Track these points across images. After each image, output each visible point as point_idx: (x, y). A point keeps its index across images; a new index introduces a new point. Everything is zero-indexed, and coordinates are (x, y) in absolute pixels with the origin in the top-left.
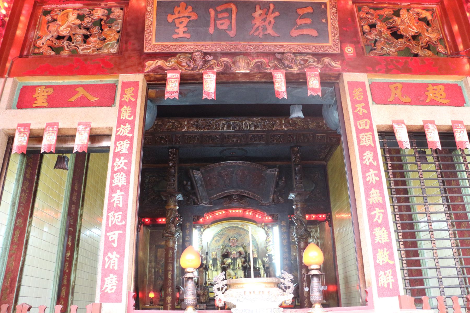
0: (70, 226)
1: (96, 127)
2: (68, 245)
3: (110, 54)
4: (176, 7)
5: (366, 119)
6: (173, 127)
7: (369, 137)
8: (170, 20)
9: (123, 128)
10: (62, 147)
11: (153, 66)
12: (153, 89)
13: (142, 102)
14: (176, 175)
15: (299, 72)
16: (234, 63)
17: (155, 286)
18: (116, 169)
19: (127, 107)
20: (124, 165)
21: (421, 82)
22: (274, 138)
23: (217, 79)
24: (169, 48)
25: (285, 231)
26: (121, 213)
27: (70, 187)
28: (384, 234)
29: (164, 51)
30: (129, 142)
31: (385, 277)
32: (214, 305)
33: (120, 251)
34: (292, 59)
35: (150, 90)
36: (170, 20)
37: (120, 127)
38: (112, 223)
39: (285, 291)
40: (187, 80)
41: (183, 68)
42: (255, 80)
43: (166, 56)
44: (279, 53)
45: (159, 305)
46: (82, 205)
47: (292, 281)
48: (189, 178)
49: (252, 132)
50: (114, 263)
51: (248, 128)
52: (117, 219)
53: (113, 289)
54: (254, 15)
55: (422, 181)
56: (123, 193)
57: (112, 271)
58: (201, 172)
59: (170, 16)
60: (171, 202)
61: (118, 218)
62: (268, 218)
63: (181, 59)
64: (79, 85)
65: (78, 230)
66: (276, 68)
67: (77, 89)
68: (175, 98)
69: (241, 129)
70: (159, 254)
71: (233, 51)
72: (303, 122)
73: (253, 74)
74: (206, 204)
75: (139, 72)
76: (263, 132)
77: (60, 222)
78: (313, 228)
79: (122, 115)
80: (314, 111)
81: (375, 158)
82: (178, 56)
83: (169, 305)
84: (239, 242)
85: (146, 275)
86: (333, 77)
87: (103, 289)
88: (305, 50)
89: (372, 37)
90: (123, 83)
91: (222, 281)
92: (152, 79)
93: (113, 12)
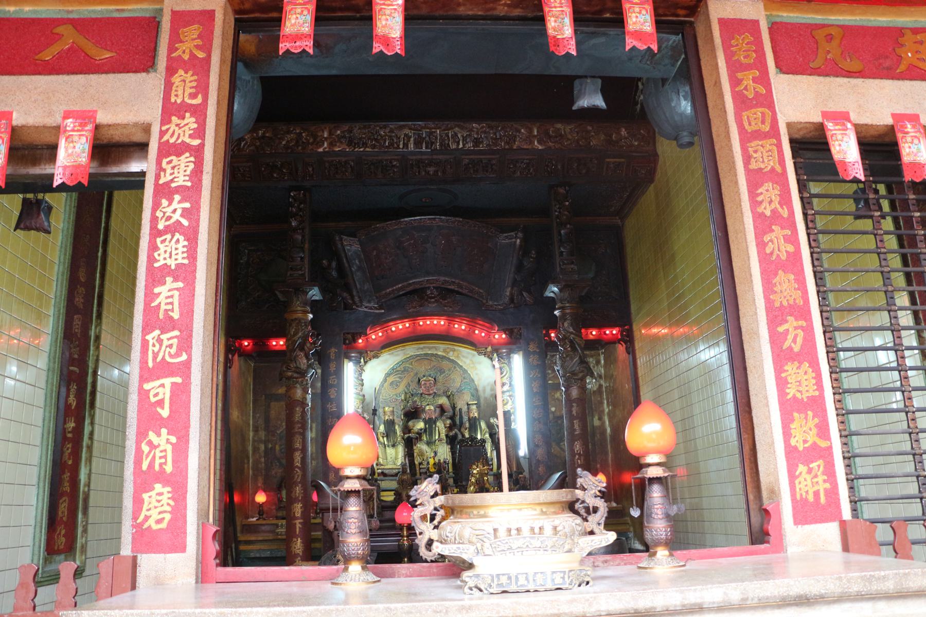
0: (72, 362)
1: (110, 123)
2: (68, 406)
5: (761, 107)
6: (297, 142)
7: (770, 151)
9: (177, 125)
10: (27, 176)
12: (250, 32)
13: (222, 61)
14: (306, 246)
17: (267, 478)
18: (161, 226)
19: (186, 73)
20: (182, 216)
21: (885, 25)
22: (515, 166)
25: (535, 363)
26: (176, 333)
27: (66, 276)
28: (806, 377)
30: (192, 159)
31: (808, 477)
32: (394, 520)
33: (178, 425)
35: (242, 37)
37: (170, 122)
38: (155, 358)
39: (586, 520)
40: (334, 10)
42: (496, 13)
45: (277, 518)
46: (99, 316)
47: (603, 495)
48: (335, 254)
49: (469, 152)
50: (165, 457)
51: (461, 146)
52: (168, 349)
53: (164, 518)
55: (882, 256)
56: (180, 285)
57: (161, 477)
58: (359, 240)
60: (297, 306)
61: (171, 346)
62: (499, 337)
64: (62, 19)
65: (90, 371)
67: (59, 30)
69: (445, 147)
70: (273, 414)
72: (578, 133)
74: (371, 309)
76: (493, 152)
77: (46, 355)
78: (592, 356)
80: (627, 95)
81: (785, 199)
83: (297, 522)
84: (439, 385)
85: (248, 458)
87: (139, 521)
91: (432, 497)
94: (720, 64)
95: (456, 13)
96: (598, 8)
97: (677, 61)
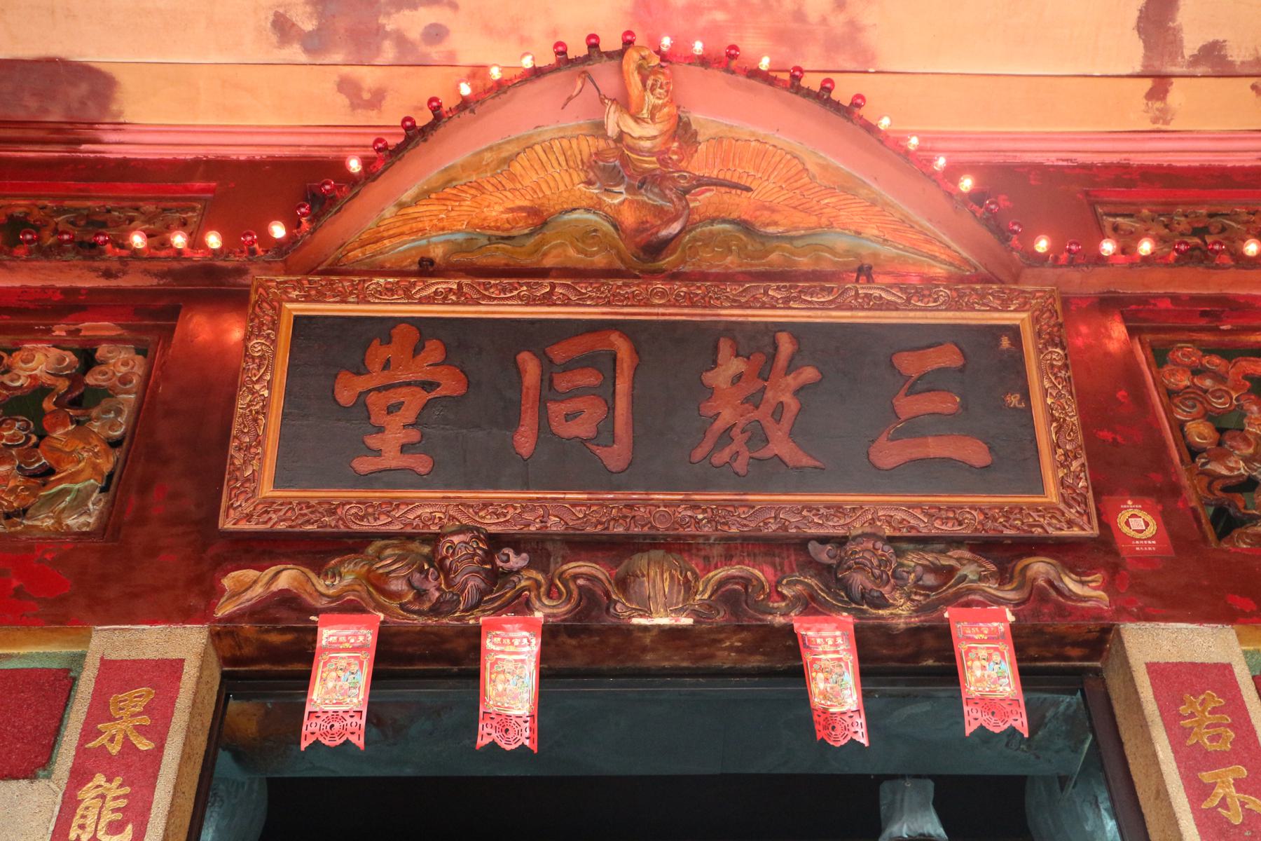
3: (62, 534)
4: (376, 342)
8: (345, 396)
11: (258, 590)
13: (185, 758)
15: (916, 621)
16: (623, 584)
19: (110, 780)
23: (543, 657)
24: (332, 512)
29: (309, 528)
34: (884, 563)
35: (233, 705)
36: (345, 396)
40: (411, 659)
41: (394, 605)
42: (715, 663)
43: (318, 549)
44: (824, 540)
54: (709, 377)
59: (344, 377)
63: (387, 563)
66: (811, 606)
68: (347, 742)
71: (620, 530)
73: (710, 631)
75: (187, 616)
79: (77, 821)
82: (371, 550)
86: (1074, 644)
88: (937, 524)
89: (1231, 469)
90: (107, 666)
92: (247, 651)
93: (102, 363)
94: (1161, 755)
95: (638, 665)
96: (909, 650)
97: (1083, 742)
